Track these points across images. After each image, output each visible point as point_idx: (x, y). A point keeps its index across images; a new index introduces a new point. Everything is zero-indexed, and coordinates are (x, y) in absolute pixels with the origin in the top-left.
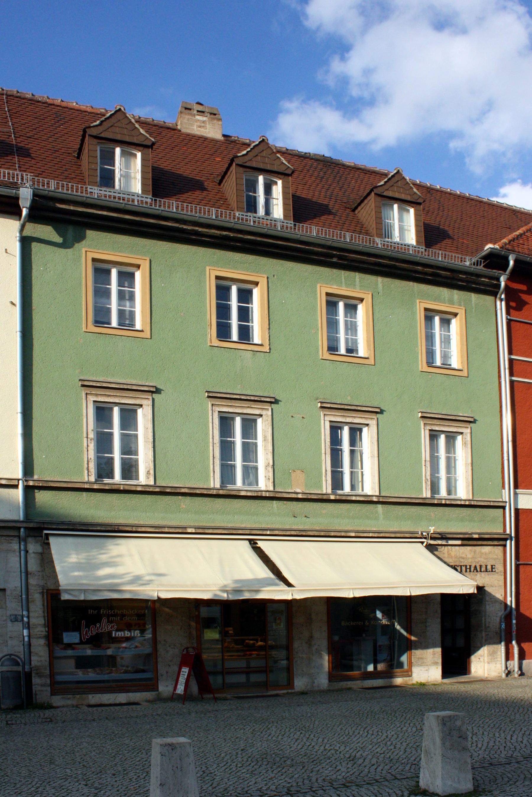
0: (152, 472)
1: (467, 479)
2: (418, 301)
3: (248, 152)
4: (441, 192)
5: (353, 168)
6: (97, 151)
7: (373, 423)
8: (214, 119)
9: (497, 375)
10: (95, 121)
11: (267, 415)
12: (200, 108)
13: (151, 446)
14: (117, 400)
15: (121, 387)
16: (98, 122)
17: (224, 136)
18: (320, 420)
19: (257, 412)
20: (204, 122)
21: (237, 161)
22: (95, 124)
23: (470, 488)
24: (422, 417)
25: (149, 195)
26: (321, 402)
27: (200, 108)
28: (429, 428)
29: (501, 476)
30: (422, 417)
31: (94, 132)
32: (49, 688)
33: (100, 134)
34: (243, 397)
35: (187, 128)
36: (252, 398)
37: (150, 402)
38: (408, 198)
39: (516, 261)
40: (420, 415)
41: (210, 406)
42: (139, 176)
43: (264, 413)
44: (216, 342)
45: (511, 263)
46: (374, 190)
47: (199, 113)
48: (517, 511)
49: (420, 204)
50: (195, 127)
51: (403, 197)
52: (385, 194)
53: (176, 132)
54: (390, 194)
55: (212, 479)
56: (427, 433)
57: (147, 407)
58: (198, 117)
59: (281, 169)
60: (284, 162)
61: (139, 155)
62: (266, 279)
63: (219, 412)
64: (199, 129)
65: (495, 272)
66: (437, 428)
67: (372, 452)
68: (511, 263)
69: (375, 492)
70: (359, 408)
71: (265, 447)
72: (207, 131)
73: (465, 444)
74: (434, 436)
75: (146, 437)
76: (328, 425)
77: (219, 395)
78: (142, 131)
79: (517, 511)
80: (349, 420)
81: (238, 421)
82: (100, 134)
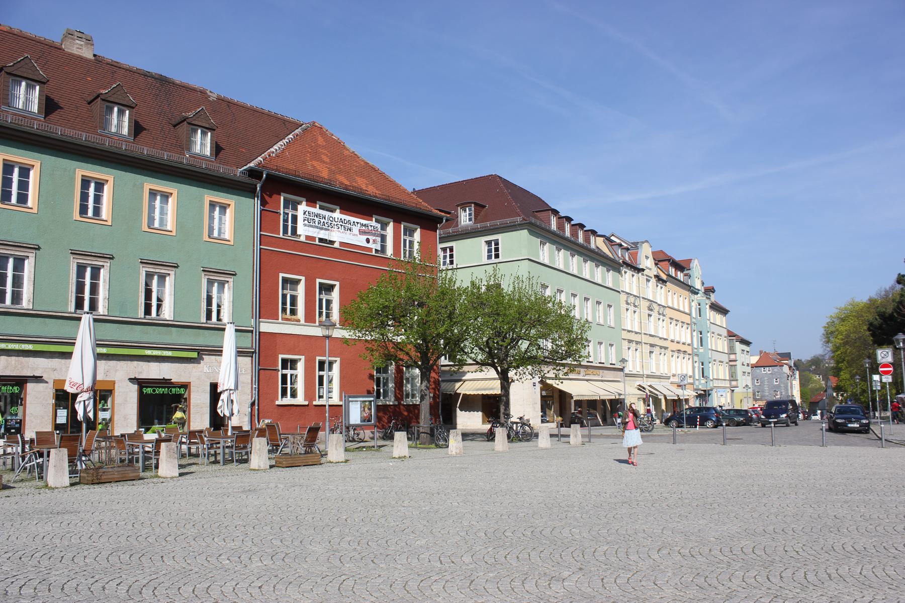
0: (32, 300)
1: (229, 311)
2: (206, 196)
3: (109, 91)
4: (237, 105)
5: (180, 86)
6: (9, 82)
7: (172, 273)
8: (88, 44)
9: (252, 244)
10: (10, 63)
11: (107, 266)
12: (80, 35)
13: (32, 283)
14: (12, 253)
15: (16, 244)
16: (12, 64)
17: (95, 55)
18: (140, 269)
19: (101, 264)
20: (81, 45)
21: (102, 97)
22: (10, 65)
23: (231, 317)
24: (203, 270)
25: (42, 115)
26: (141, 259)
27: (80, 35)
28: (207, 277)
29: (251, 310)
30: (203, 270)
31: (8, 70)
32: (380, 238)
33: (13, 71)
34: (93, 254)
35: (69, 49)
36: (99, 255)
37: (34, 255)
38: (207, 126)
39: (267, 175)
40: (202, 269)
41: (72, 258)
42: (37, 101)
43: (105, 264)
44: (79, 218)
45: (264, 175)
46: (187, 120)
47: (78, 38)
48: (260, 332)
49: (214, 130)
50: (75, 49)
51: (204, 125)
52: (193, 123)
53: (61, 51)
54: (196, 123)
55: (69, 306)
56: (206, 280)
57: (32, 258)
58: (77, 41)
59: (129, 104)
60: (131, 99)
61: (38, 88)
62: (113, 178)
63: (77, 263)
64: (78, 50)
65: (254, 181)
66: (212, 278)
67: (171, 292)
68: (264, 175)
69: (171, 317)
70: (164, 264)
71: (104, 286)
72: (83, 51)
73: (229, 288)
74: (210, 283)
75: (29, 277)
76: (144, 273)
77: (78, 252)
78: (41, 72)
79: (260, 332)
80: (157, 271)
81: (89, 270)
82: (13, 71)
